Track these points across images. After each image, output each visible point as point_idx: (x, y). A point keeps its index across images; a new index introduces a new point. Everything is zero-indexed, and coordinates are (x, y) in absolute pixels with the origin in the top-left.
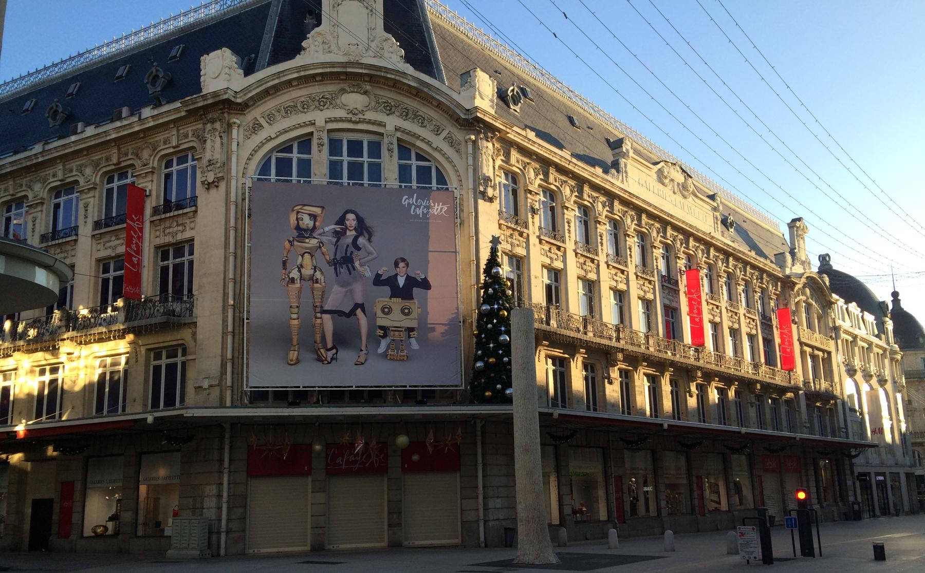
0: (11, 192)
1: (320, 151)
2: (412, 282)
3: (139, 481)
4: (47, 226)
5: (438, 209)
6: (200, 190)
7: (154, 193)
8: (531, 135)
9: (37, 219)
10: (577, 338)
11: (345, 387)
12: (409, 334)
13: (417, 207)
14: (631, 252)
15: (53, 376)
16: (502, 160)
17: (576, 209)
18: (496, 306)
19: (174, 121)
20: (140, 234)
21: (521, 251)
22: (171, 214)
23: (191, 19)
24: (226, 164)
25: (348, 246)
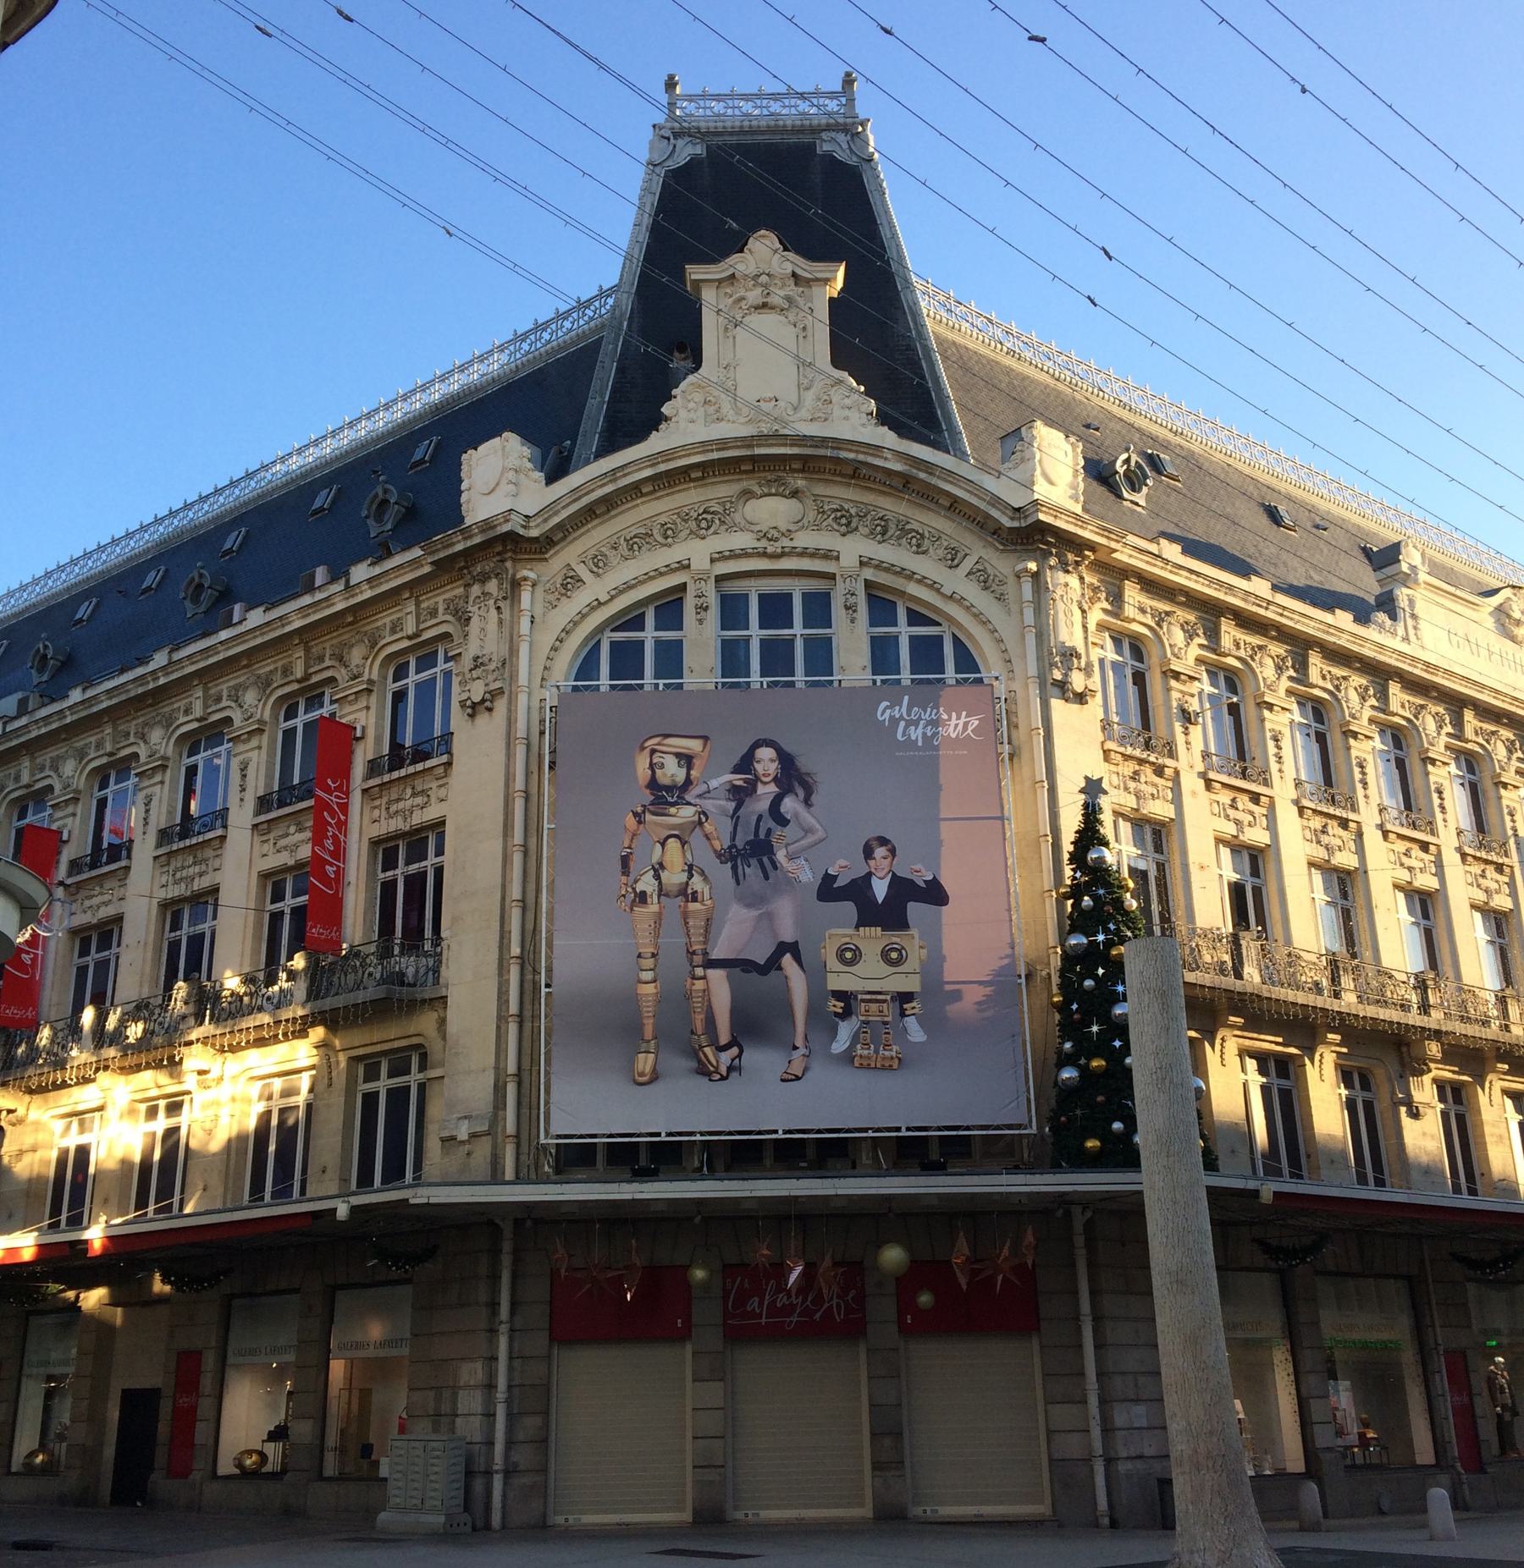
0: (108, 748)
1: (701, 621)
2: (903, 889)
3: (329, 1351)
4: (171, 813)
5: (957, 724)
6: (458, 719)
7: (371, 733)
8: (1172, 551)
9: (154, 798)
10: (1349, 1014)
11: (760, 1133)
12: (901, 1007)
13: (909, 723)
14: (1442, 799)
15: (171, 1122)
16: (1105, 611)
17: (1295, 707)
18: (1101, 938)
19: (410, 586)
20: (342, 818)
21: (1161, 809)
22: (403, 772)
23: (455, 385)
24: (508, 663)
25: (760, 818)
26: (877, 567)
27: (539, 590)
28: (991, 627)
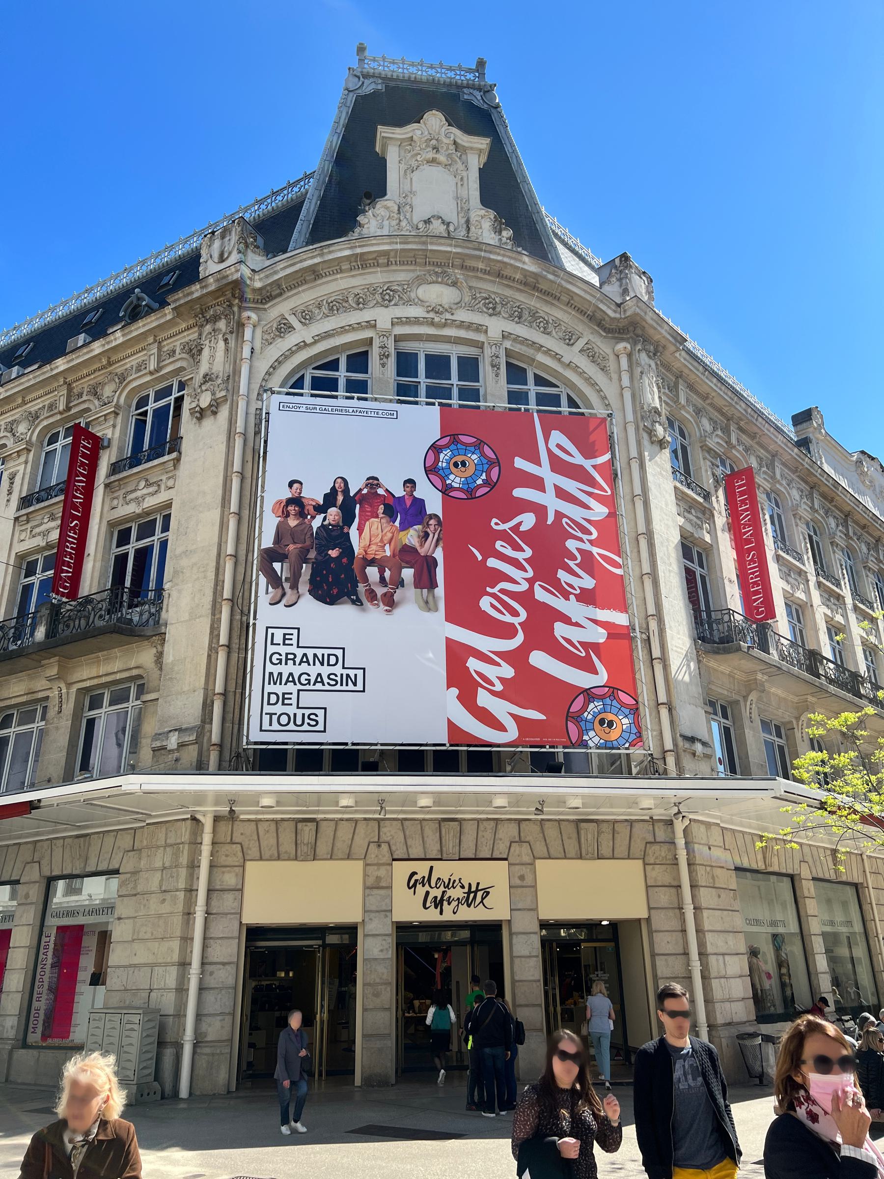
1: (383, 365)
24: (232, 378)
26: (515, 340)
27: (259, 332)
28: (598, 388)
